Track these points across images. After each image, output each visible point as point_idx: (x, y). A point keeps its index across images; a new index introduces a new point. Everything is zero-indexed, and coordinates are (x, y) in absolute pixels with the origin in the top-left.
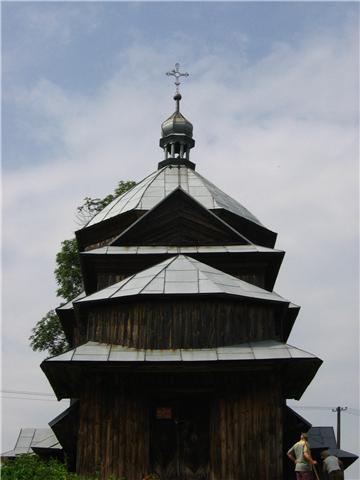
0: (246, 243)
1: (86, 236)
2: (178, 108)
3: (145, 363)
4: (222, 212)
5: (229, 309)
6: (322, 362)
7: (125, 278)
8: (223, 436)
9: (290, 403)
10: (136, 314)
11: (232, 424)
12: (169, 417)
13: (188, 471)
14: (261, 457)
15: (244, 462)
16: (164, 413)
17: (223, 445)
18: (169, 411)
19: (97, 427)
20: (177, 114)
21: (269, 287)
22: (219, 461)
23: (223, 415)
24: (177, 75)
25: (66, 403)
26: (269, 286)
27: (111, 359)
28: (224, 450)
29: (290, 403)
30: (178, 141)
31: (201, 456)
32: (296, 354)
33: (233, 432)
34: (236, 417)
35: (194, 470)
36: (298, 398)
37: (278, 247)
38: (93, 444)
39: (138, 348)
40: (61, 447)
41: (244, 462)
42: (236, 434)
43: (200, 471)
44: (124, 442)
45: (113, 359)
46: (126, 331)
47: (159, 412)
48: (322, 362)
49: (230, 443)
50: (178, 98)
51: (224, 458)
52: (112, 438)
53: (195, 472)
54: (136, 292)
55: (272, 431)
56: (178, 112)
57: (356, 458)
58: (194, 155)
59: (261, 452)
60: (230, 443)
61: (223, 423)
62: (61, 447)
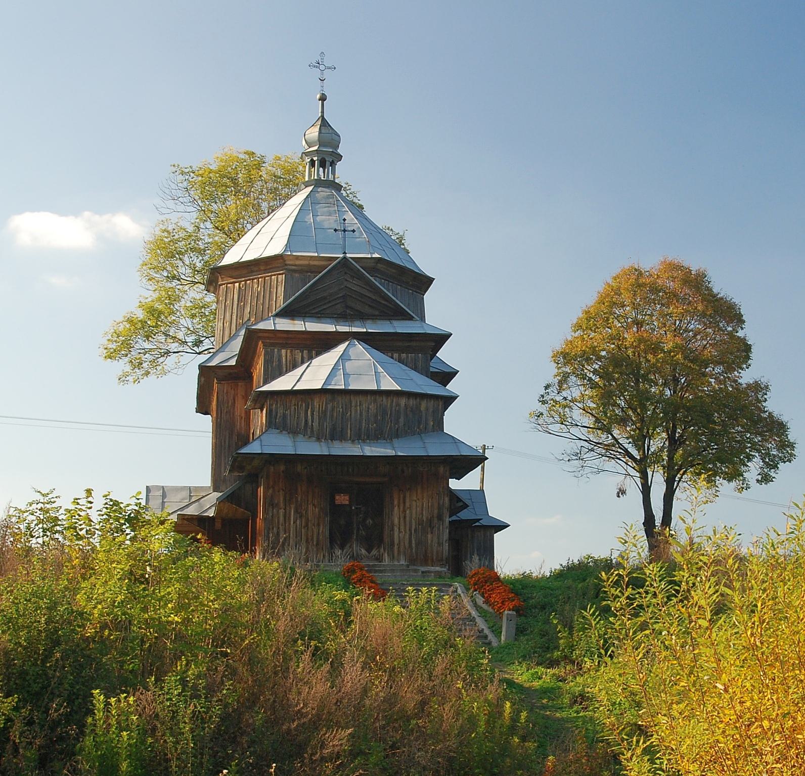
2: (323, 112)
5: (403, 401)
8: (396, 521)
10: (316, 404)
11: (404, 511)
12: (347, 503)
13: (363, 551)
14: (429, 542)
15: (414, 545)
16: (342, 499)
17: (396, 529)
18: (347, 498)
19: (282, 512)
20: (324, 124)
22: (392, 544)
23: (396, 502)
24: (322, 67)
28: (396, 533)
33: (405, 517)
34: (407, 505)
38: (279, 528)
41: (414, 545)
42: (408, 519)
44: (307, 525)
46: (306, 421)
47: (337, 497)
49: (402, 527)
50: (323, 99)
51: (396, 541)
53: (369, 553)
55: (440, 518)
56: (322, 116)
59: (429, 536)
60: (402, 527)
61: (396, 508)
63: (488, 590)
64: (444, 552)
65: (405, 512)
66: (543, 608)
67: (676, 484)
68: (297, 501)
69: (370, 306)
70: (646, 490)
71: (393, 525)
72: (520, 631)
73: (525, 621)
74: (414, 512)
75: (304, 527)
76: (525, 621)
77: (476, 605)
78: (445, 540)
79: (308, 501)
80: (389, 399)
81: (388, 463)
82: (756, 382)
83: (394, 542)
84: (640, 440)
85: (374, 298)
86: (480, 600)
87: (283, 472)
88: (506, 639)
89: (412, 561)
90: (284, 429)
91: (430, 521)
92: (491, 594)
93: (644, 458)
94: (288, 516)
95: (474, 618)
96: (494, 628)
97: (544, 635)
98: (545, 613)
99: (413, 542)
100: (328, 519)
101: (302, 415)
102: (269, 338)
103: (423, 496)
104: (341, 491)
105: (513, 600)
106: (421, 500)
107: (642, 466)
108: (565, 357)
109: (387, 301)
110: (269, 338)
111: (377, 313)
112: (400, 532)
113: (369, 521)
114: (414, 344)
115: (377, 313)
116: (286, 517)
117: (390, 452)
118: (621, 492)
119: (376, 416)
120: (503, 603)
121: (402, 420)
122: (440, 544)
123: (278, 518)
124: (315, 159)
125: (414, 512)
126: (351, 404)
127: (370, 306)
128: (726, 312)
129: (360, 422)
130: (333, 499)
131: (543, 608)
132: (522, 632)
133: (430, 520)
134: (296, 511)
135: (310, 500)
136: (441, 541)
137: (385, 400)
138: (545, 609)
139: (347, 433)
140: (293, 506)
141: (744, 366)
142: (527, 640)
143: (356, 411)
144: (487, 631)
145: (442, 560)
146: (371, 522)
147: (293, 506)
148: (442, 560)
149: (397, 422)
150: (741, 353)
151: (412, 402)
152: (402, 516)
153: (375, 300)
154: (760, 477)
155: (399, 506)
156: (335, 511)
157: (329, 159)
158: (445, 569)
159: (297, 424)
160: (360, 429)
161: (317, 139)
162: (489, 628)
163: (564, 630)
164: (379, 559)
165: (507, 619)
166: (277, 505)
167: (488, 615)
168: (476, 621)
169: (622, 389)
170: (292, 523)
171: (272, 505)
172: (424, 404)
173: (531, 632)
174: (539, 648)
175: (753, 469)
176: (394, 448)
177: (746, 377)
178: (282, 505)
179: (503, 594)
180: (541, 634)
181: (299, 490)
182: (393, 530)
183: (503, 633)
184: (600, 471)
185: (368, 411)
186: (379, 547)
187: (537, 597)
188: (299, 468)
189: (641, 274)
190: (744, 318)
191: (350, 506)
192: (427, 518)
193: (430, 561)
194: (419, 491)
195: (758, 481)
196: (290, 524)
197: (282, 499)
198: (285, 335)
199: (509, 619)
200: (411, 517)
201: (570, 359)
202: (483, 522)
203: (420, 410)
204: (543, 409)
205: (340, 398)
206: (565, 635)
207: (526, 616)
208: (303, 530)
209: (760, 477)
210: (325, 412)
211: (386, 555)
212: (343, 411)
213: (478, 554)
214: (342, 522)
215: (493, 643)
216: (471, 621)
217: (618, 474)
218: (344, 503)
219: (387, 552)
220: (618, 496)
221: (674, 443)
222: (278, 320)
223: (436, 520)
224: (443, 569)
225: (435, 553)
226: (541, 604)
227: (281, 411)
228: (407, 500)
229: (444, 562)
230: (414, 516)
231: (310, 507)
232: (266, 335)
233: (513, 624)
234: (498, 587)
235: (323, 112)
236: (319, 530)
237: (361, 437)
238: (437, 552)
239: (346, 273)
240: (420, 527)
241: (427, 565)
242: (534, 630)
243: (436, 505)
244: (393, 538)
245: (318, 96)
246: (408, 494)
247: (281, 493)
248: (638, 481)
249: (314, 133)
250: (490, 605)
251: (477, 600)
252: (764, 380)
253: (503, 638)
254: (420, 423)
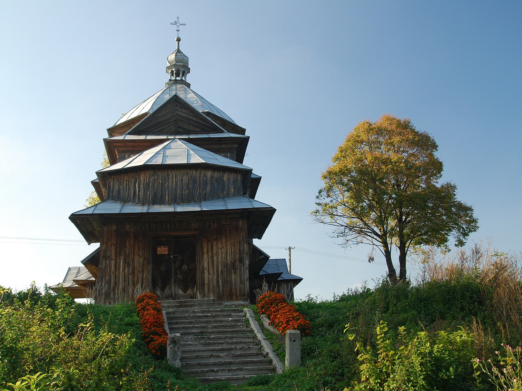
0: (222, 132)
1: (112, 131)
2: (178, 47)
3: (148, 213)
4: (208, 114)
5: (209, 174)
6: (274, 210)
7: (135, 155)
8: (206, 265)
9: (256, 242)
10: (142, 178)
11: (212, 257)
12: (167, 253)
13: (181, 292)
14: (233, 280)
15: (221, 284)
16: (163, 250)
17: (206, 272)
18: (167, 249)
19: (113, 262)
20: (179, 51)
21: (241, 161)
22: (203, 284)
23: (205, 250)
24: (178, 24)
25: (96, 246)
26: (244, 134)
27: (122, 212)
28: (206, 275)
29: (256, 242)
30: (180, 69)
31: (190, 281)
32: (257, 206)
33: (213, 262)
34: (215, 251)
35: (185, 291)
36: (260, 238)
37: (247, 134)
38: (110, 276)
39: (143, 204)
40: (94, 279)
41: (221, 284)
42: (215, 263)
43: (189, 292)
44: (133, 272)
45: (123, 212)
46: (135, 192)
47: (159, 249)
48: (274, 210)
49: (211, 270)
50: (179, 40)
51: (206, 282)
52: (124, 270)
53: (185, 293)
54: (142, 163)
55: (241, 260)
56: (178, 49)
57: (301, 279)
58: (189, 78)
59: (233, 276)
60: (211, 270)
61: (205, 255)
62: (94, 279)
63: (274, 311)
64: (246, 288)
65: (213, 258)
66: (331, 326)
67: (406, 249)
68: (125, 253)
69: (194, 126)
70: (388, 255)
71: (203, 268)
72: (307, 353)
73: (312, 341)
74: (220, 257)
75: (131, 274)
76: (312, 341)
77: (262, 326)
78: (246, 278)
79: (134, 253)
80: (198, 172)
81: (198, 220)
82: (448, 184)
83: (204, 282)
84: (381, 221)
85: (196, 120)
86: (266, 322)
87: (115, 230)
88: (290, 364)
89: (220, 297)
90: (118, 200)
91: (233, 264)
92: (276, 315)
93: (385, 234)
94: (118, 266)
95: (259, 341)
96: (278, 351)
97: (336, 358)
98: (334, 332)
99: (220, 281)
100: (150, 266)
101: (132, 188)
102: (121, 147)
103: (226, 244)
104: (161, 244)
105: (298, 319)
106: (225, 247)
107: (383, 238)
108: (330, 175)
109: (206, 122)
110: (121, 147)
111: (198, 130)
112: (209, 274)
113: (185, 267)
114: (224, 146)
115: (198, 130)
116: (117, 267)
117: (197, 209)
118: (371, 259)
119: (188, 185)
120: (287, 322)
121: (208, 188)
122: (241, 282)
123: (110, 267)
124: (174, 70)
125: (220, 257)
126: (168, 177)
127: (194, 126)
128: (426, 143)
129: (176, 192)
130: (155, 251)
131: (331, 326)
132: (309, 354)
133: (233, 264)
134: (125, 261)
135: (136, 252)
136: (243, 279)
137: (193, 173)
138: (332, 327)
139: (166, 198)
140: (122, 257)
141: (438, 175)
142: (315, 364)
143: (172, 182)
144: (271, 355)
145: (245, 295)
146: (186, 267)
147: (122, 257)
148: (245, 295)
149: (205, 189)
150: (437, 167)
151: (216, 174)
152: (210, 261)
153: (197, 122)
154: (457, 243)
155: (208, 253)
156: (157, 260)
157: (182, 70)
158: (247, 303)
159: (128, 195)
160: (176, 195)
161: (174, 59)
162: (274, 351)
163: (365, 349)
164: (193, 297)
165: (291, 340)
166: (110, 257)
167: (275, 337)
168: (262, 344)
169: (367, 188)
170: (121, 271)
171: (105, 257)
172: (226, 176)
173: (320, 353)
174: (331, 375)
175: (452, 238)
176: (201, 206)
177: (439, 183)
178: (113, 257)
179: (288, 314)
180: (331, 356)
181: (128, 245)
182: (203, 272)
183: (287, 357)
184: (358, 243)
185: (182, 181)
186: (193, 288)
187: (324, 316)
188: (128, 227)
189: (370, 125)
190: (437, 144)
191: (169, 255)
192: (231, 262)
193: (234, 297)
194: (224, 241)
195: (456, 245)
196: (119, 272)
197: (113, 252)
198: (132, 144)
199: (293, 340)
200: (218, 262)
201: (334, 177)
202: (284, 277)
203: (223, 180)
204: (320, 208)
205: (160, 173)
206: (367, 356)
207: (312, 336)
208: (130, 277)
209: (457, 243)
210: (148, 184)
211: (198, 293)
212: (162, 182)
213: (267, 282)
214: (163, 268)
215: (277, 369)
216: (256, 345)
217: (370, 246)
218: (164, 253)
219: (198, 290)
220: (370, 262)
221: (401, 223)
222: (128, 136)
223: (238, 263)
224: (246, 303)
225: (238, 290)
226: (327, 322)
227: (116, 188)
228: (215, 248)
229: (246, 297)
230: (220, 261)
231: (136, 257)
232: (118, 144)
233: (298, 343)
234: (283, 307)
235: (178, 47)
236: (143, 276)
237: (175, 201)
238: (240, 289)
239: (177, 106)
240: (225, 269)
241: (232, 299)
242: (322, 351)
243: (237, 252)
244: (204, 278)
245: (176, 39)
246: (215, 243)
247: (113, 248)
248: (382, 249)
249: (172, 57)
250: (276, 326)
251: (264, 322)
252: (452, 183)
253: (287, 363)
254: (223, 190)
